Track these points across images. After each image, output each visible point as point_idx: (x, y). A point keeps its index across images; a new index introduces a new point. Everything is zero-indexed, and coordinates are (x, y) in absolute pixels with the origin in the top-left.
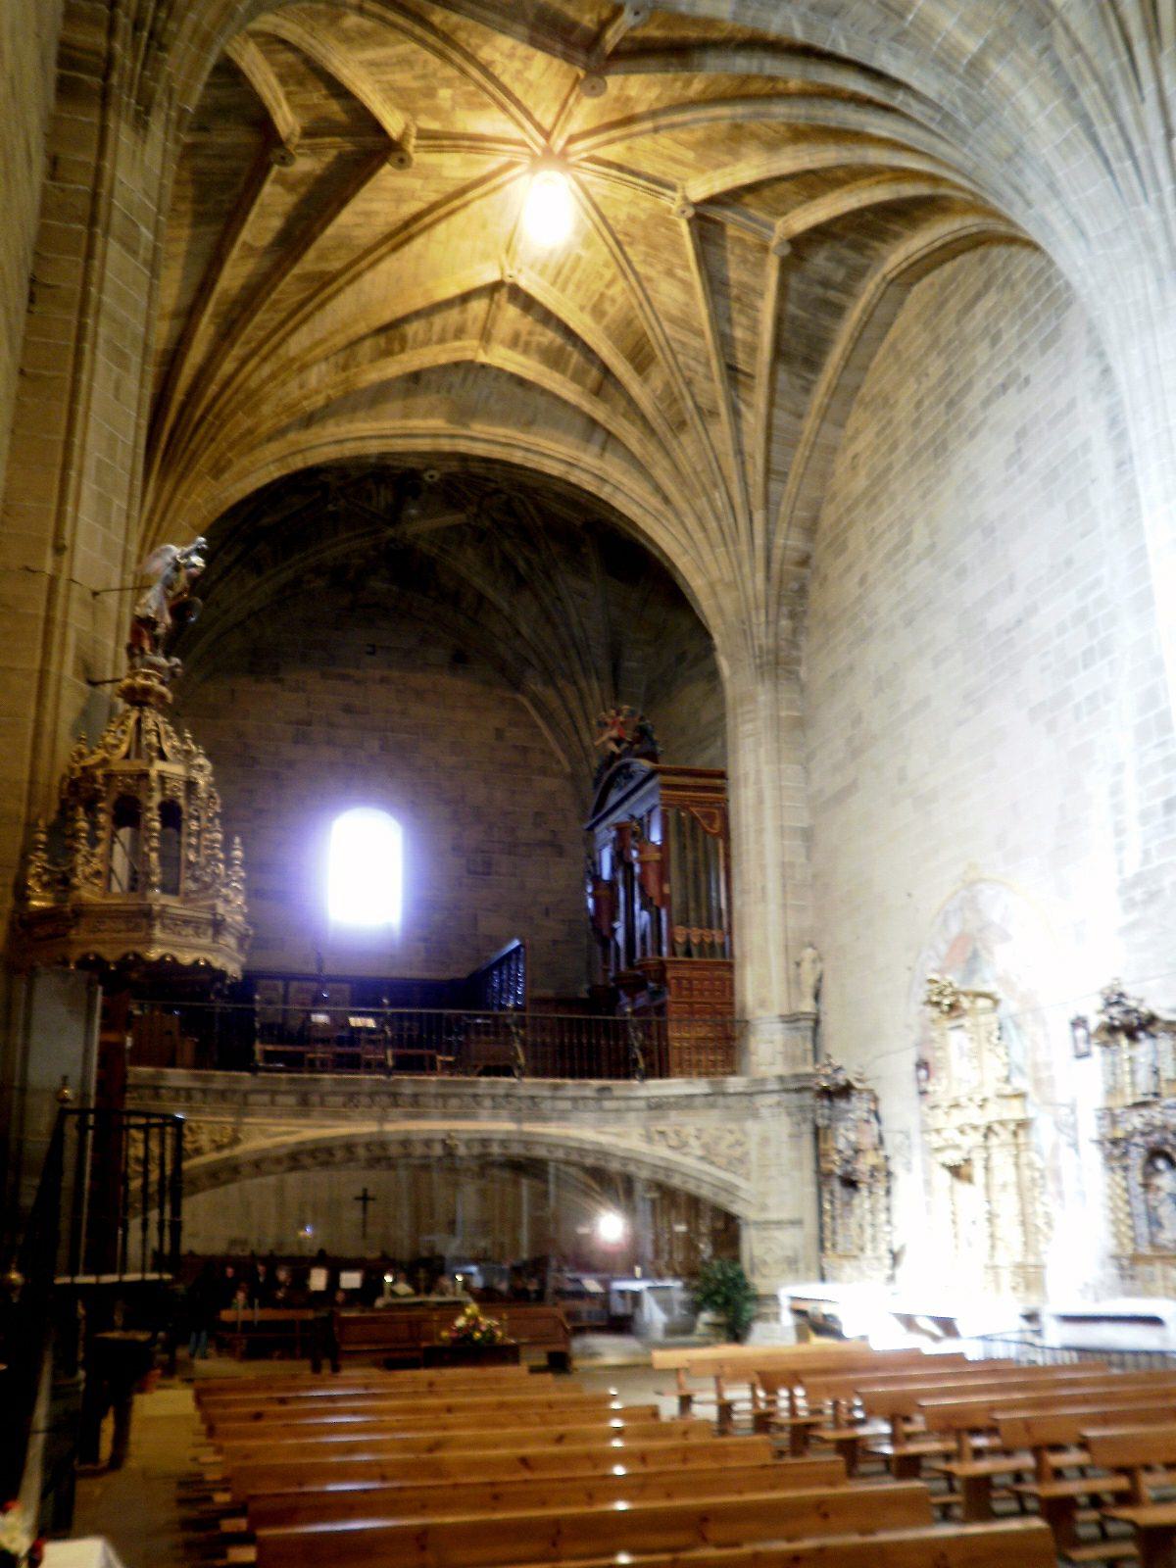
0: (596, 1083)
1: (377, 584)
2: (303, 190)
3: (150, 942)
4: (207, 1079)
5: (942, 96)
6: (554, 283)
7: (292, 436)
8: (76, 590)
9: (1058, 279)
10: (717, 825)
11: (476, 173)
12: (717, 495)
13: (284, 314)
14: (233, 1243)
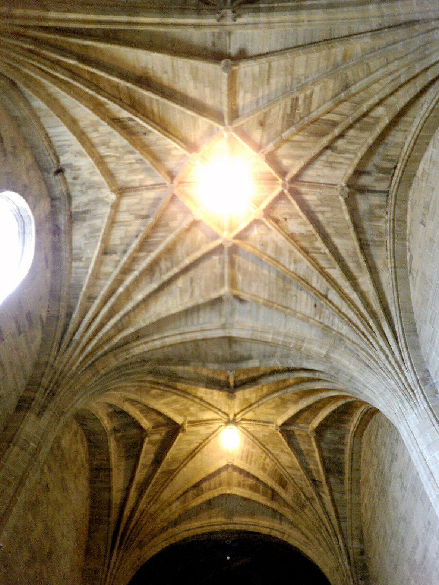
2: (158, 445)
5: (325, 370)
6: (247, 462)
7: (170, 530)
9: (219, 358)
11: (211, 431)
12: (323, 531)
13: (160, 486)
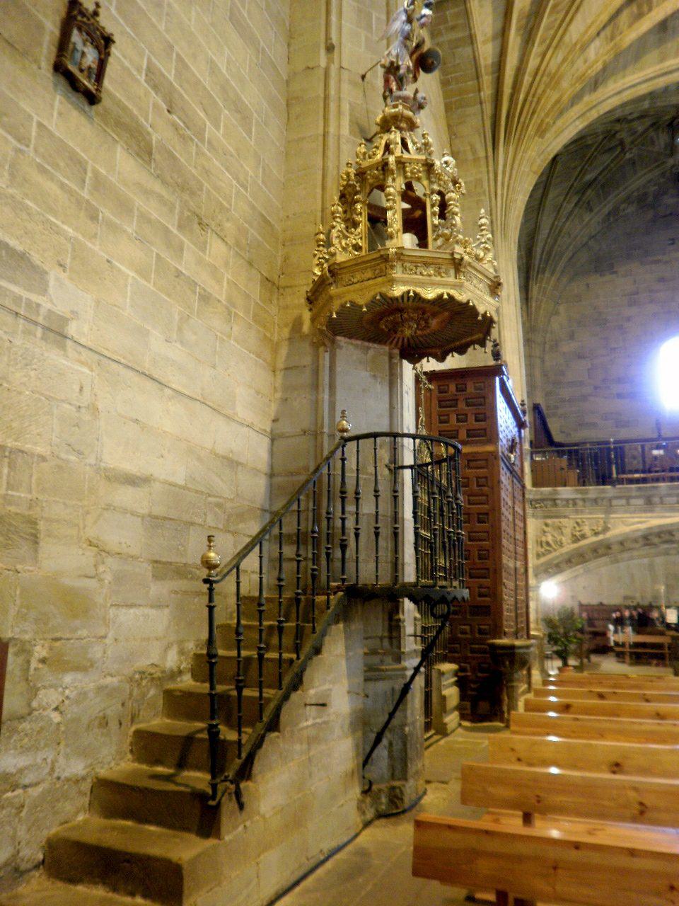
3: (392, 282)
4: (586, 492)
7: (586, 99)
8: (345, 75)
14: (626, 598)
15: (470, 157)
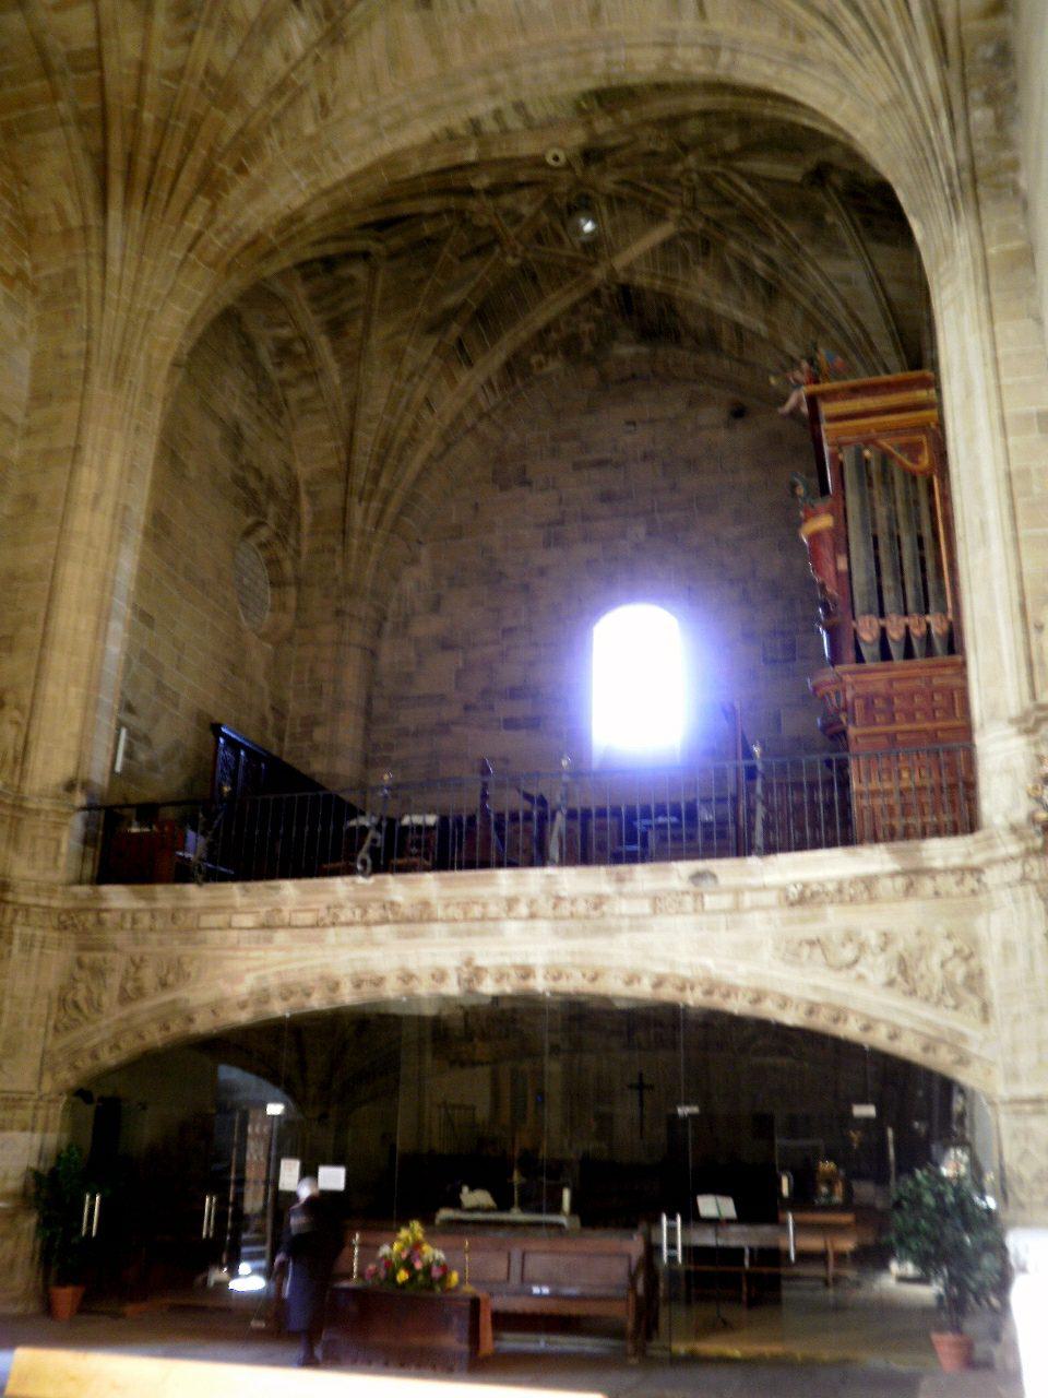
0: (684, 868)
1: (625, 350)
10: (925, 460)
15: (57, 227)
